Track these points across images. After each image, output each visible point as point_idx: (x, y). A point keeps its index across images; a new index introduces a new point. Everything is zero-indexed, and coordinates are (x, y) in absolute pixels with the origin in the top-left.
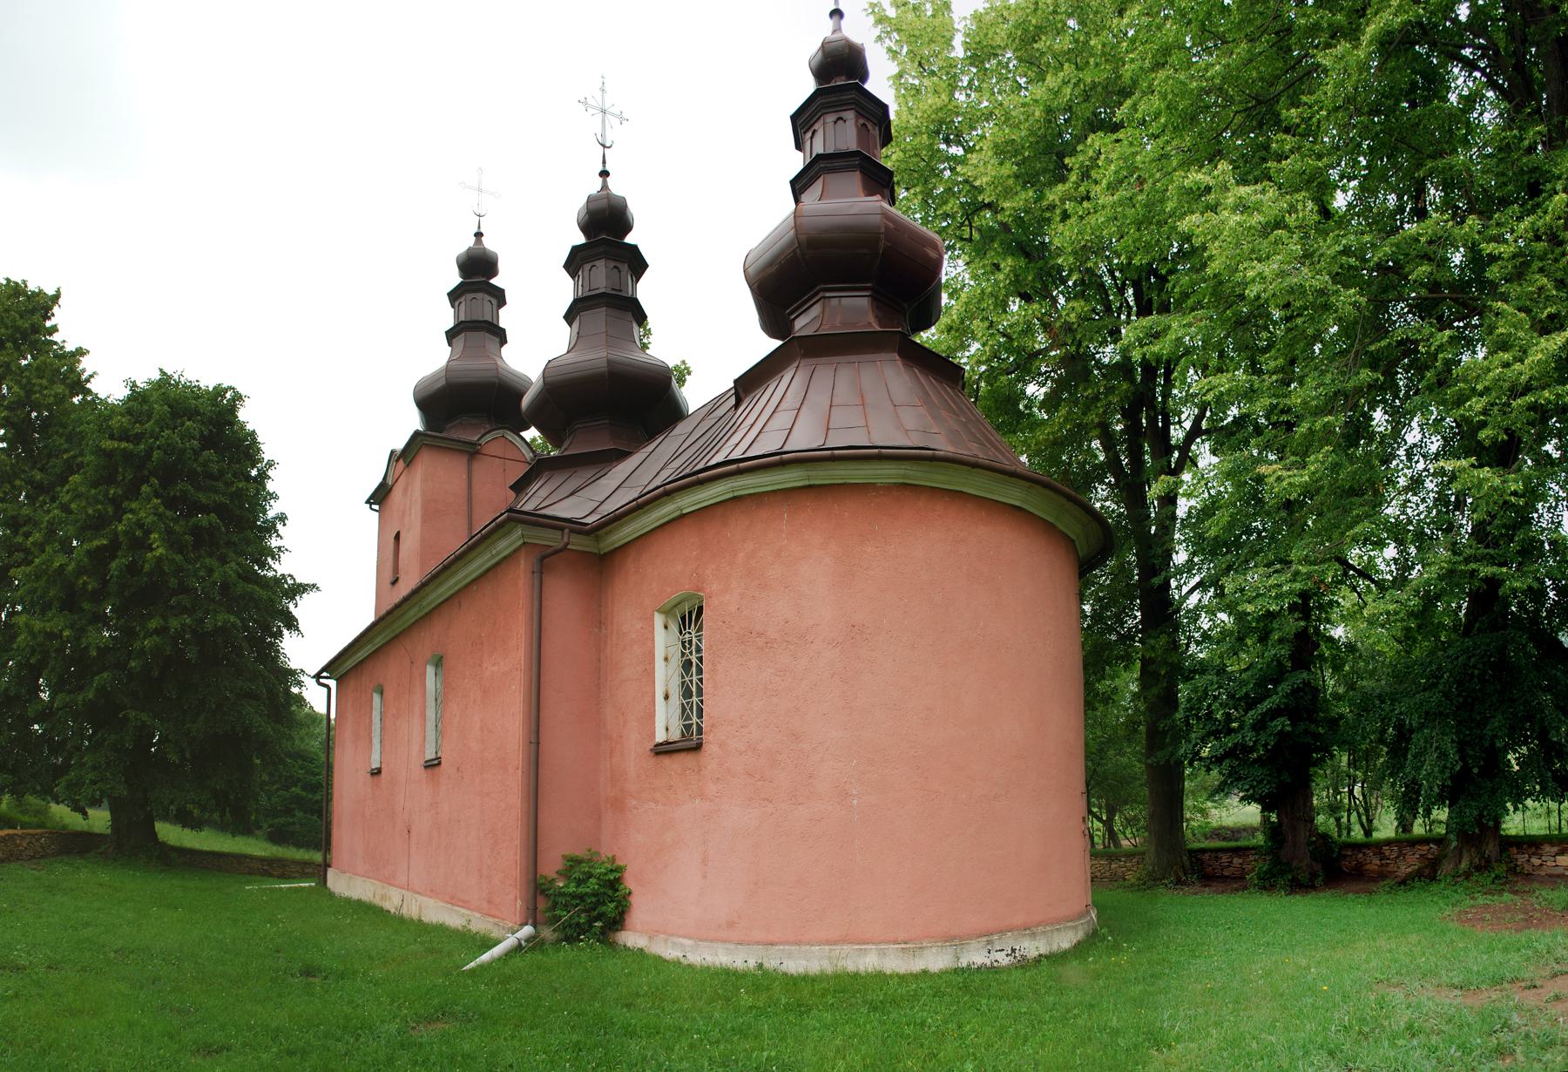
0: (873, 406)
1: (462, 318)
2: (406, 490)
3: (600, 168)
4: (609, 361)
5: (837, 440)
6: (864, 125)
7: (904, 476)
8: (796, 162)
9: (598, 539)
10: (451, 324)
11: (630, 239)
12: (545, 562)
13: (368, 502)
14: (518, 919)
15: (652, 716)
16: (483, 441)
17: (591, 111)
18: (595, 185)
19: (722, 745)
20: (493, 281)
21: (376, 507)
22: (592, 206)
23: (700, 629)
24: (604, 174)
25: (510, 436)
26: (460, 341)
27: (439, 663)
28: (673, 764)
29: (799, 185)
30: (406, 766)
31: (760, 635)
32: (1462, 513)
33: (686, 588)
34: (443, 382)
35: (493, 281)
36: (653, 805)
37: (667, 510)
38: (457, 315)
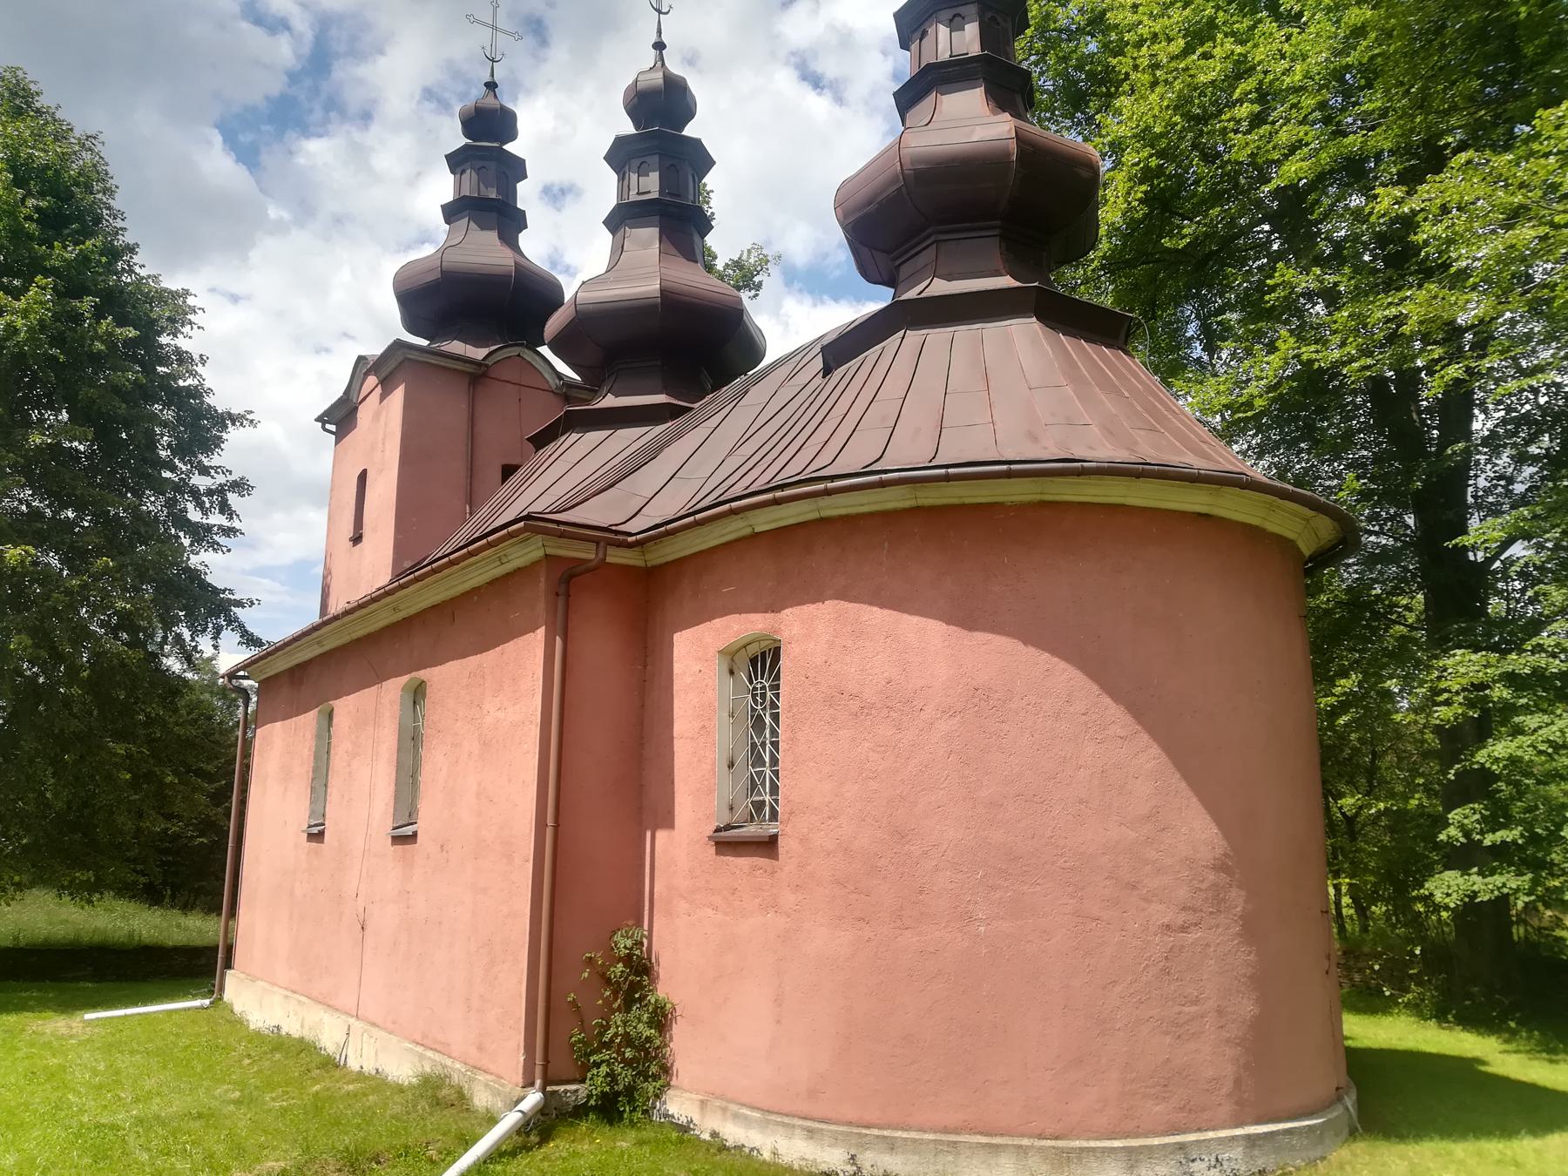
2: (377, 416)
3: (654, 38)
5: (952, 453)
6: (993, 19)
8: (903, 64)
10: (448, 196)
11: (689, 131)
19: (803, 840)
20: (508, 147)
21: (333, 428)
23: (777, 677)
24: (659, 46)
25: (528, 355)
29: (909, 96)
31: (853, 696)
32: (1477, 821)
35: (508, 147)
36: (710, 912)
38: (458, 186)
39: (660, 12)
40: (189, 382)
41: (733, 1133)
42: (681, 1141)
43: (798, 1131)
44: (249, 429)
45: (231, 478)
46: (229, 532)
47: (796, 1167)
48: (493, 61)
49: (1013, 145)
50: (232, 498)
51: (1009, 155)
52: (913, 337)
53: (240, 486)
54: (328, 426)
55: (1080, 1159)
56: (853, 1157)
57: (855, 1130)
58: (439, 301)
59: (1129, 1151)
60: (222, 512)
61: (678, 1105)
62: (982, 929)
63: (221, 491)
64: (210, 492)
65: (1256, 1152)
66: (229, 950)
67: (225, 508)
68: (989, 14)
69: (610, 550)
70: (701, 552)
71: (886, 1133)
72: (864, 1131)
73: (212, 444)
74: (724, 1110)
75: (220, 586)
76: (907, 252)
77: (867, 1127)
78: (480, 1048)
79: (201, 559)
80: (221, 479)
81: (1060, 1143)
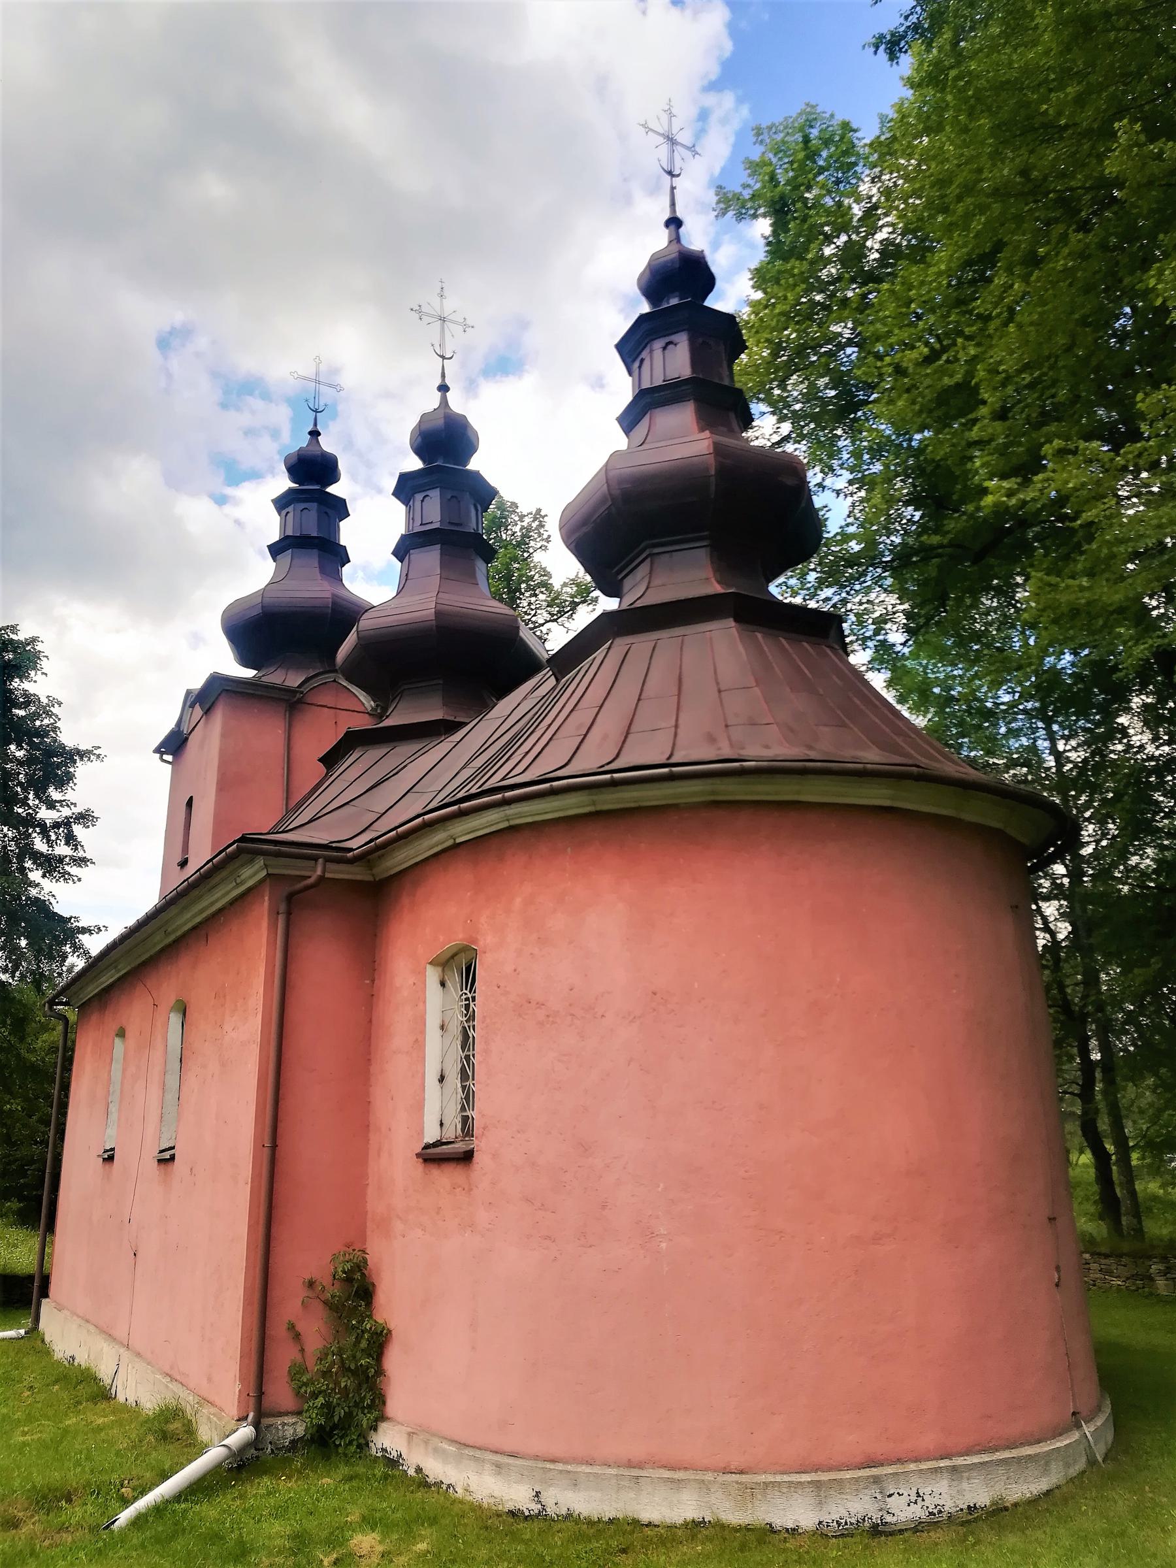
0: (703, 697)
1: (289, 533)
3: (438, 382)
4: (438, 614)
7: (713, 793)
9: (370, 866)
10: (275, 537)
11: (474, 464)
12: (295, 903)
13: (157, 750)
14: (233, 1410)
15: (420, 1106)
16: (305, 689)
17: (426, 319)
18: (432, 402)
19: (495, 1156)
20: (332, 489)
21: (169, 758)
22: (424, 427)
26: (286, 557)
27: (183, 1010)
28: (445, 1177)
30: (138, 1157)
31: (540, 1005)
33: (459, 938)
34: (258, 611)
35: (332, 489)
37: (438, 839)
38: (284, 526)
39: (443, 357)
40: (46, 722)
41: (435, 1469)
42: (386, 1477)
43: (487, 1466)
44: (96, 764)
45: (76, 810)
46: (82, 862)
47: (485, 1505)
48: (316, 411)
49: (711, 460)
50: (77, 829)
51: (707, 469)
52: (620, 645)
53: (85, 818)
54: (166, 757)
55: (764, 1495)
56: (538, 1494)
57: (540, 1465)
58: (261, 631)
59: (817, 1485)
60: (68, 843)
61: (388, 1439)
62: (664, 1245)
63: (67, 823)
64: (56, 825)
65: (965, 1485)
66: (45, 1280)
67: (70, 839)
68: (700, 340)
69: (330, 866)
70: (416, 864)
71: (569, 1468)
72: (552, 1466)
73: (64, 780)
74: (426, 1442)
75: (66, 915)
76: (632, 561)
77: (553, 1461)
78: (210, 1380)
79: (44, 886)
80: (66, 812)
81: (744, 1478)
